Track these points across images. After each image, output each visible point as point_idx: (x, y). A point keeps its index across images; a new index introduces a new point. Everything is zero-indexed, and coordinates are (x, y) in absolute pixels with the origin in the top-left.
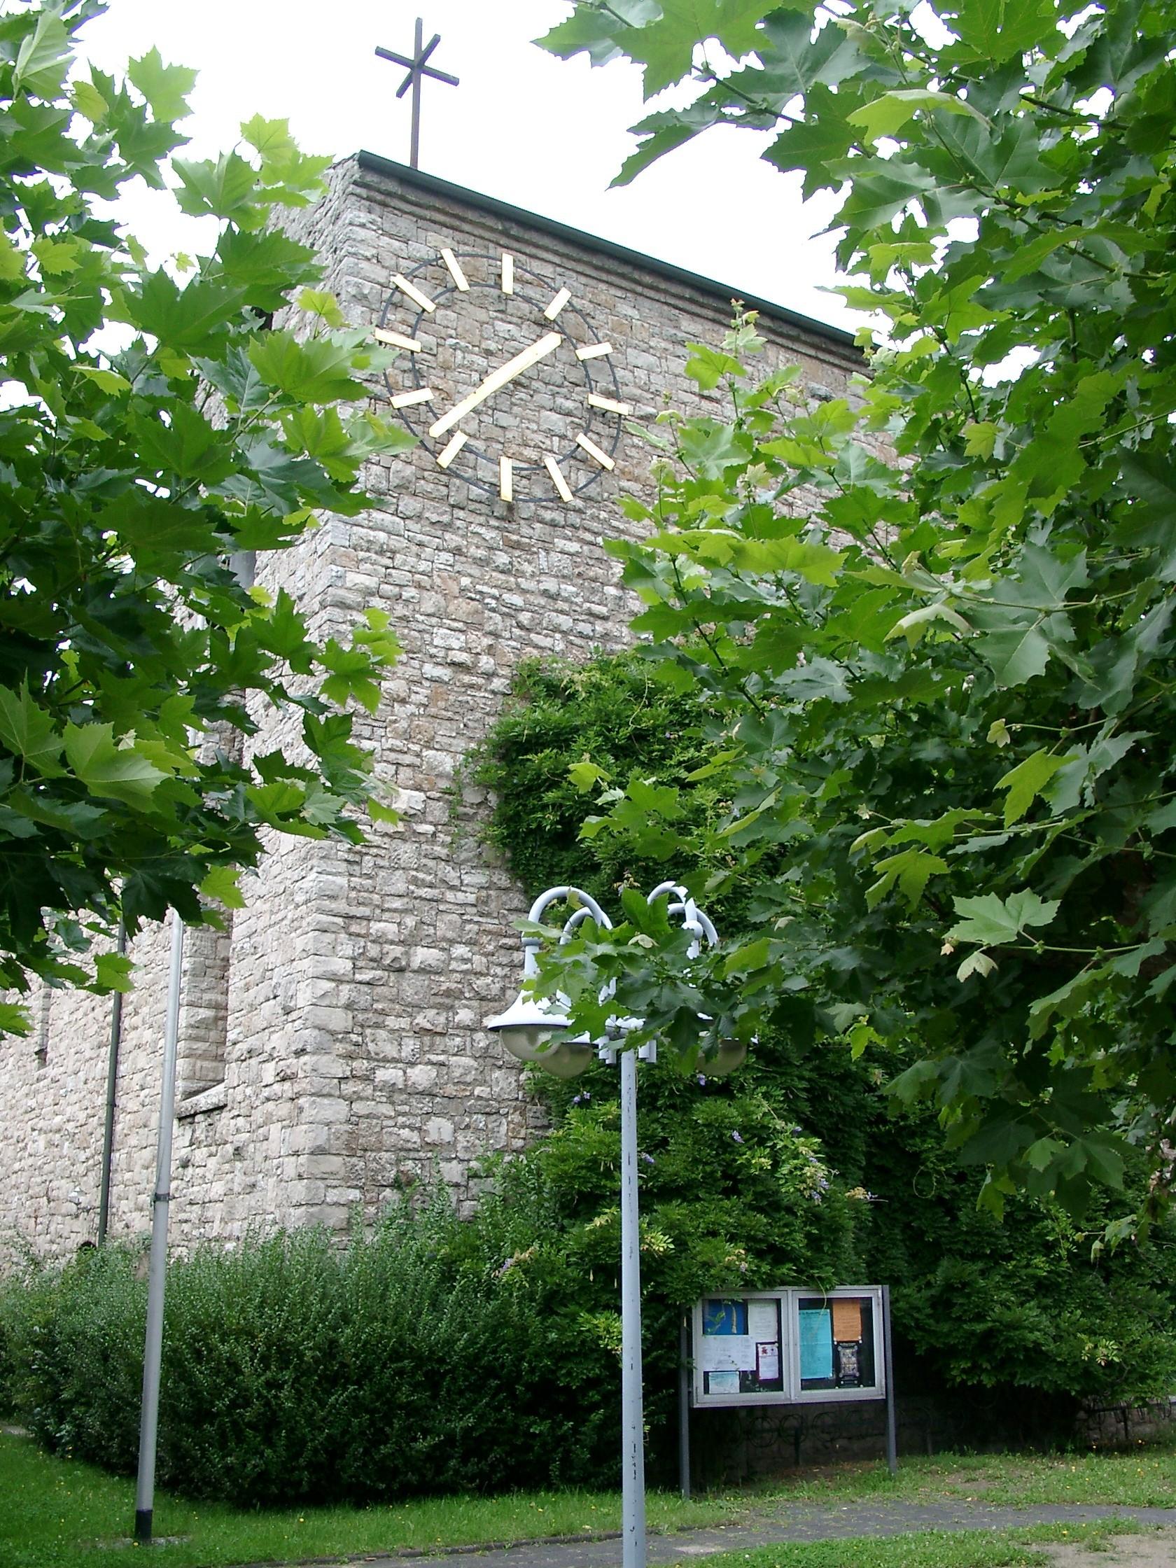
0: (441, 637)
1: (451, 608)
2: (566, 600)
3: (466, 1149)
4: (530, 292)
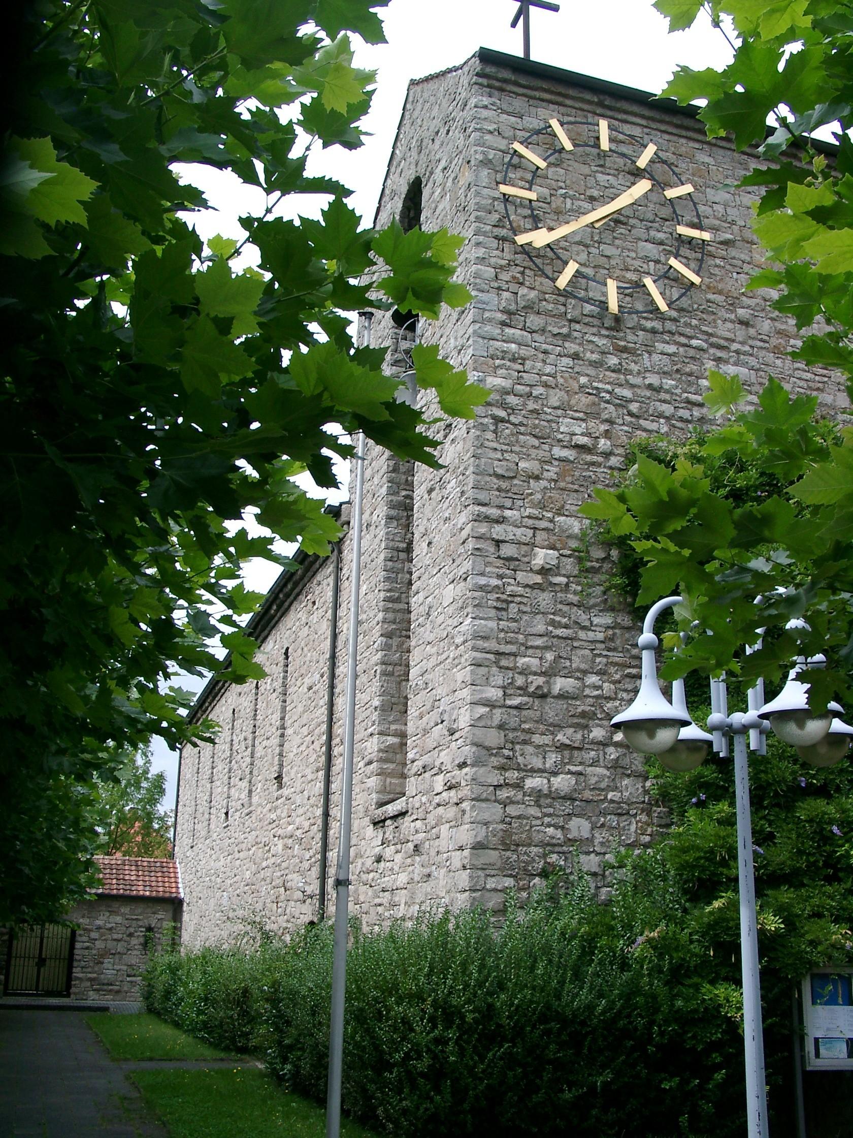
0: (566, 425)
1: (573, 402)
2: (667, 391)
3: (602, 844)
4: (623, 149)
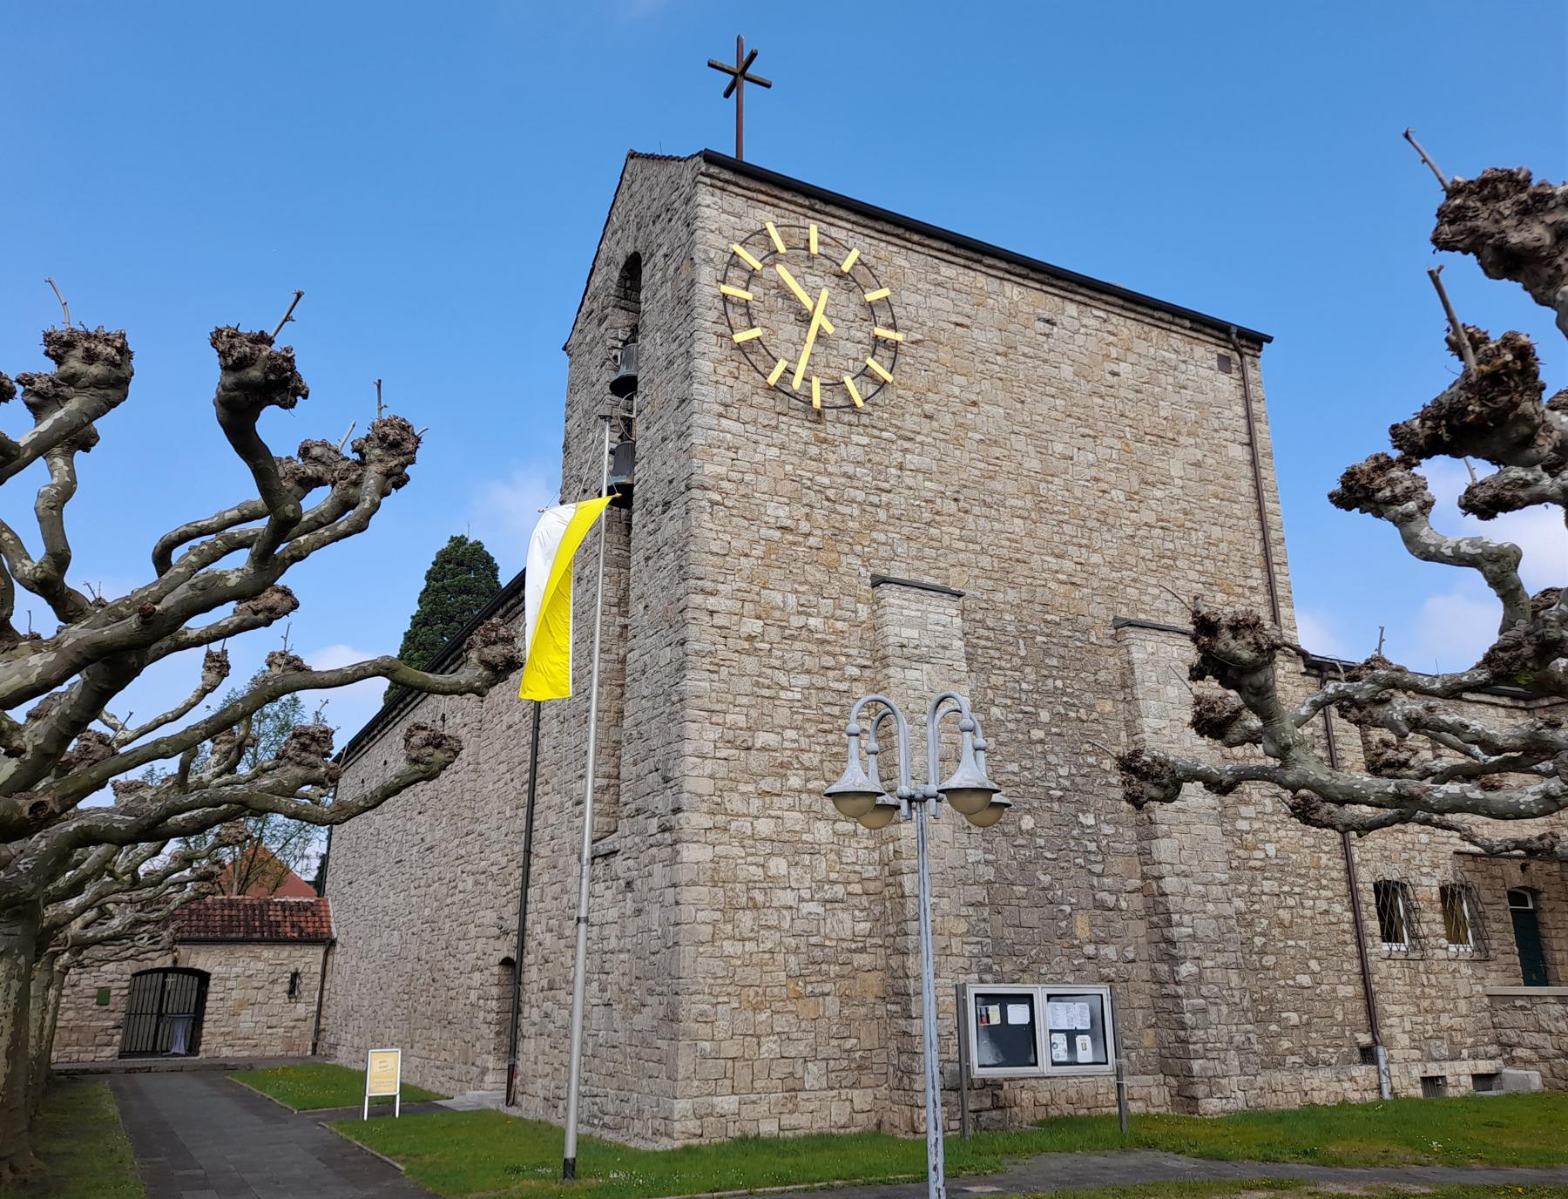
4: (830, 252)
